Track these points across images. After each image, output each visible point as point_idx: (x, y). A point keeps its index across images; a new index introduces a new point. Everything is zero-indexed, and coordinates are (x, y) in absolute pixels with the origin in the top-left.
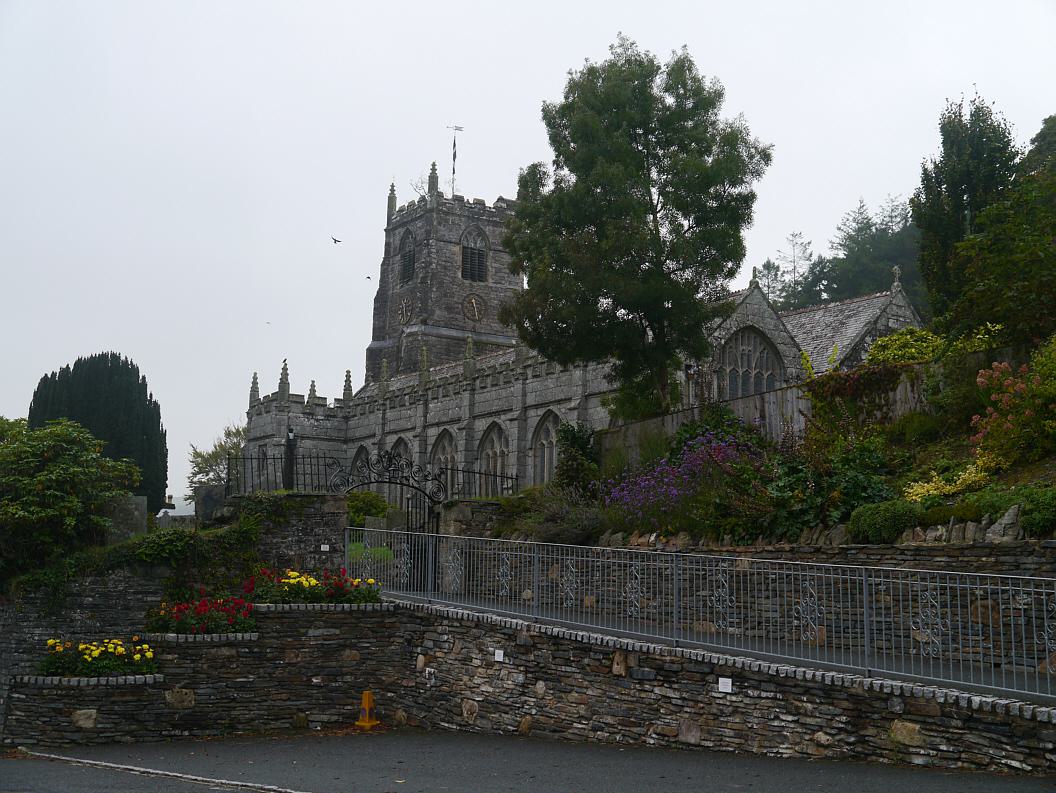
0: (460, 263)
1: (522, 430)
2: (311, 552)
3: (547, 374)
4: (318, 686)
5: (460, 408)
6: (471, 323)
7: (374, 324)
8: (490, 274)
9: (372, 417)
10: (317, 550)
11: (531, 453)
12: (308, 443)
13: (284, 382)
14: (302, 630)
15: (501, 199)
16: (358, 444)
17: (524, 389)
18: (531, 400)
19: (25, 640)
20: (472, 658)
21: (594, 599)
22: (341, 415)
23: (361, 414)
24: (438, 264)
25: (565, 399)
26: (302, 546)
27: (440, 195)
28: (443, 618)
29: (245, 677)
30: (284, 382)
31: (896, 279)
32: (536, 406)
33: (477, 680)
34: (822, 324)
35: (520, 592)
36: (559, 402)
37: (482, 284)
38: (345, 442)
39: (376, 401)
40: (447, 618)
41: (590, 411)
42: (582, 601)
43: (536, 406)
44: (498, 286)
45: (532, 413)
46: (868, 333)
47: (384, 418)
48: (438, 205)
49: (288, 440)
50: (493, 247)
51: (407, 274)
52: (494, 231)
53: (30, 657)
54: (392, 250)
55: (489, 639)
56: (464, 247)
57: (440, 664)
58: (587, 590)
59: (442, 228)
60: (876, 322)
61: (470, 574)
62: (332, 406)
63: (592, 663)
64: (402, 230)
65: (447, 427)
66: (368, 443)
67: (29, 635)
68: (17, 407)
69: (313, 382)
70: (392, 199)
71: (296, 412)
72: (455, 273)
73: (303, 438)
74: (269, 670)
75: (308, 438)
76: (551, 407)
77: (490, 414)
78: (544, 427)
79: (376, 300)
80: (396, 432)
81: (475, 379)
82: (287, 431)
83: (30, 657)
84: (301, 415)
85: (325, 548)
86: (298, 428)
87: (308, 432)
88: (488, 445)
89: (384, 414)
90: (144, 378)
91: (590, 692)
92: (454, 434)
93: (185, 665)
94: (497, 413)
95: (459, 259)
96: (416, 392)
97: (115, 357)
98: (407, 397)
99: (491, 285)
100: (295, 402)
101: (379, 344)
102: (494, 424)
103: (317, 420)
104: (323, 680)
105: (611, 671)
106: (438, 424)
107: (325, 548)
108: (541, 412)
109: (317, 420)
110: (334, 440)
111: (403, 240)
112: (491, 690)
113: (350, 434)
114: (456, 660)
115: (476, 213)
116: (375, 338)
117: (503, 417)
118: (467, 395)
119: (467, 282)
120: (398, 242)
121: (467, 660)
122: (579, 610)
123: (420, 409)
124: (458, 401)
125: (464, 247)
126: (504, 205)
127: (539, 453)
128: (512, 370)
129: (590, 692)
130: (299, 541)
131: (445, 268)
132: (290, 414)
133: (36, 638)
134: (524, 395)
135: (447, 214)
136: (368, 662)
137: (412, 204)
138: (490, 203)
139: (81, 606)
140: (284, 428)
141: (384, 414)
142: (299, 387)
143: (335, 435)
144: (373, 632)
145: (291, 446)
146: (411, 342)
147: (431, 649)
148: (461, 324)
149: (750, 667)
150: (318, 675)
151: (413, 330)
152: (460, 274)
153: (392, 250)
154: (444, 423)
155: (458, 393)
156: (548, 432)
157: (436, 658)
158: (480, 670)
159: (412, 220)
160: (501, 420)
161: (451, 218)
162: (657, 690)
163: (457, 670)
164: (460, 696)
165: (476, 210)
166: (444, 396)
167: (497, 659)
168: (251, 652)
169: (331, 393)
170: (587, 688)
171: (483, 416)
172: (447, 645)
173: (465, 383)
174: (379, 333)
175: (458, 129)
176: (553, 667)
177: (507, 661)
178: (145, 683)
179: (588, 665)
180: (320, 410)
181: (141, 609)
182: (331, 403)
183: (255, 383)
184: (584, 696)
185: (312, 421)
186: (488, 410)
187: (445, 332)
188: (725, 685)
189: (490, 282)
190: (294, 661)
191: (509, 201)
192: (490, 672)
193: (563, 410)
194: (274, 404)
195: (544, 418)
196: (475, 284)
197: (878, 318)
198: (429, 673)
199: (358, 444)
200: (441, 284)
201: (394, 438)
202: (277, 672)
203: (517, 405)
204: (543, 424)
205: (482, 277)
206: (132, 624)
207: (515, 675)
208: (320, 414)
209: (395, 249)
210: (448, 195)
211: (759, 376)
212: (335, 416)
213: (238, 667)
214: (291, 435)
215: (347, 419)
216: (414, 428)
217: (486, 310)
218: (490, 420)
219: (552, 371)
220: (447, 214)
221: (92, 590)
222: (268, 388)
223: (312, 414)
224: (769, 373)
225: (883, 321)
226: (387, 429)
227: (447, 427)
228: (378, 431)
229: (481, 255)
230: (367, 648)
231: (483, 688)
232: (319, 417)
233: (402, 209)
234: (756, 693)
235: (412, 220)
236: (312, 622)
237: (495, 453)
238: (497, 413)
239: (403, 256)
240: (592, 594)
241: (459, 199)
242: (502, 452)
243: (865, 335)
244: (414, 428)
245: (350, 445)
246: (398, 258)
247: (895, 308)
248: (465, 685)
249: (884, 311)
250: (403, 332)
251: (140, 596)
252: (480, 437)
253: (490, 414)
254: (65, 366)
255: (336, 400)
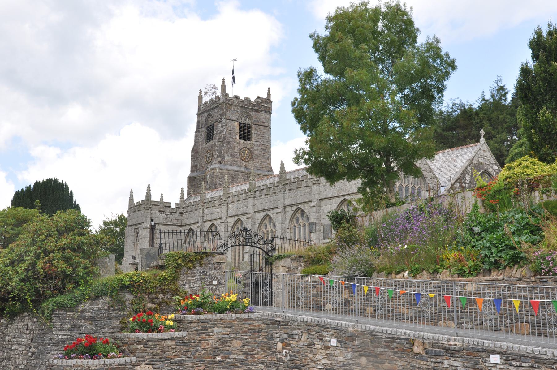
0: (238, 131)
1: (284, 218)
2: (207, 285)
3: (297, 188)
4: (220, 362)
5: (247, 207)
6: (244, 163)
7: (191, 164)
8: (254, 137)
9: (196, 212)
10: (210, 284)
11: (288, 231)
12: (162, 227)
13: (148, 195)
14: (210, 330)
15: (258, 98)
16: (188, 227)
17: (284, 197)
18: (288, 202)
19: (54, 339)
20: (314, 345)
21: (372, 309)
22: (178, 212)
23: (190, 211)
24: (226, 132)
25: (308, 202)
26: (203, 281)
27: (227, 95)
28: (293, 320)
29: (181, 357)
30: (148, 195)
31: (482, 137)
32: (291, 206)
33: (318, 357)
34: (442, 161)
35: (324, 305)
36: (304, 203)
37: (249, 142)
38: (181, 226)
39: (198, 204)
40: (297, 321)
41: (322, 208)
42: (365, 310)
43: (291, 206)
44: (258, 143)
45: (288, 209)
46: (469, 165)
47: (203, 213)
48: (226, 101)
49: (151, 225)
50: (255, 123)
51: (210, 136)
52: (255, 115)
53: (56, 348)
54: (200, 125)
55: (326, 333)
56: (240, 123)
57: (293, 348)
58: (368, 304)
59: (228, 112)
60: (473, 159)
61: (292, 296)
62: (174, 207)
63: (399, 346)
64: (206, 114)
65: (240, 217)
66: (194, 227)
67: (56, 336)
68: (2, 210)
69: (162, 194)
70: (131, 199)
71: (155, 210)
72: (235, 137)
73: (158, 224)
74: (193, 353)
75: (162, 224)
76: (300, 206)
77: (265, 210)
78: (296, 216)
79: (193, 151)
80: (210, 221)
81: (255, 192)
82: (150, 220)
83: (56, 348)
84: (158, 212)
85: (215, 282)
86: (156, 219)
87: (161, 221)
88: (263, 226)
89: (203, 211)
90: (71, 192)
91: (398, 363)
92: (244, 221)
93: (147, 351)
94: (268, 210)
95: (237, 128)
96: (222, 199)
97: (56, 181)
98: (216, 202)
99: (254, 143)
100: (155, 205)
101: (195, 174)
102: (239, 219)
103: (166, 215)
104: (222, 358)
105: (412, 351)
106: (234, 216)
107: (215, 282)
108: (294, 208)
109: (166, 215)
110: (175, 225)
111: (207, 119)
112: (329, 362)
113: (184, 222)
114: (303, 345)
115: (246, 105)
116: (192, 171)
117: (272, 211)
118: (251, 200)
119: (242, 141)
120: (204, 121)
121: (311, 345)
122: (362, 313)
123: (225, 208)
124: (246, 203)
125: (240, 123)
126: (260, 101)
127: (293, 231)
128: (277, 186)
129: (398, 363)
130: (201, 279)
131: (230, 134)
132: (152, 212)
133: (60, 337)
134: (284, 200)
135: (231, 105)
136: (246, 347)
137: (211, 100)
138: (253, 100)
139: (84, 318)
140: (149, 220)
141: (203, 211)
142: (155, 198)
143: (175, 222)
144: (249, 329)
145: (153, 228)
146: (213, 173)
147: (286, 339)
148: (239, 163)
149: (512, 348)
150: (219, 355)
151: (214, 167)
152: (238, 137)
153: (200, 125)
154: (238, 215)
155: (246, 199)
156: (298, 220)
157: (290, 344)
158: (320, 351)
159: (212, 109)
160: (271, 213)
161: (233, 108)
162: (446, 362)
163: (304, 351)
164: (308, 366)
165: (246, 103)
166: (237, 201)
167: (332, 344)
168: (183, 342)
169: (173, 199)
170: (396, 361)
171: (260, 211)
172: (297, 337)
173: (250, 193)
174: (194, 168)
175: (235, 60)
176: (371, 349)
177: (340, 346)
178: (126, 363)
179: (397, 348)
180: (167, 209)
181: (118, 319)
182: (173, 206)
183: (131, 195)
184: (395, 366)
185: (164, 215)
186: (263, 208)
187: (230, 167)
188: (495, 359)
189: (253, 140)
190: (207, 347)
191: (263, 98)
192: (328, 352)
193: (307, 207)
194: (143, 206)
195: (296, 212)
196: (245, 142)
197: (474, 157)
198: (286, 353)
199: (188, 227)
200: (228, 142)
201: (209, 224)
202: (197, 354)
203: (280, 205)
204: (295, 215)
205: (249, 139)
206: (112, 328)
207: (346, 354)
208: (168, 211)
209: (202, 124)
210: (231, 95)
211: (413, 188)
212: (175, 213)
213: (176, 352)
214: (153, 223)
215: (182, 213)
216: (221, 218)
217: (252, 156)
218: (265, 213)
219: (300, 186)
220: (231, 105)
221: (91, 308)
222: (139, 197)
223: (164, 212)
224: (419, 186)
225: (476, 159)
226: (205, 219)
227: (240, 217)
228: (200, 220)
229: (249, 127)
230: (246, 339)
231: (323, 361)
232: (167, 213)
233: (206, 103)
234: (518, 363)
235: (212, 109)
236: (215, 324)
237: (300, 225)
238: (268, 210)
239: (207, 128)
240: (371, 306)
241: (237, 97)
242: (272, 231)
243: (467, 166)
244: (221, 218)
245: (184, 228)
246: (204, 129)
247: (482, 152)
248: (311, 359)
249: (477, 153)
250: (207, 168)
251: (117, 311)
252: (259, 222)
253: (265, 210)
254: (28, 186)
255: (176, 204)
